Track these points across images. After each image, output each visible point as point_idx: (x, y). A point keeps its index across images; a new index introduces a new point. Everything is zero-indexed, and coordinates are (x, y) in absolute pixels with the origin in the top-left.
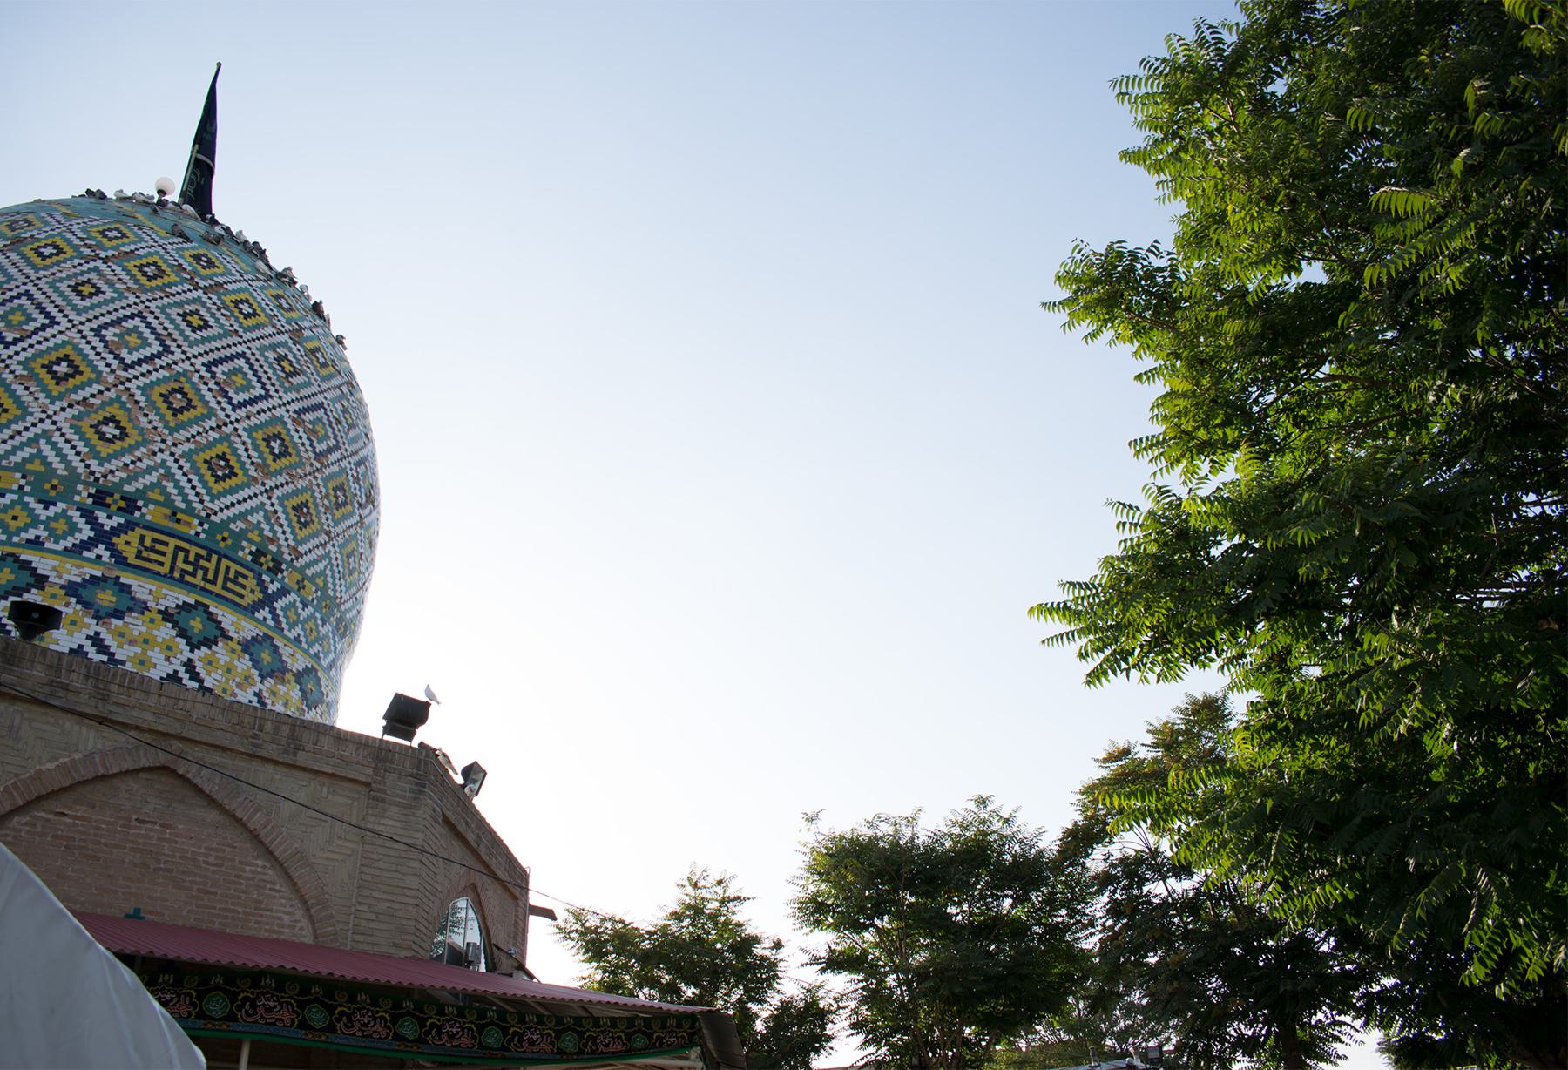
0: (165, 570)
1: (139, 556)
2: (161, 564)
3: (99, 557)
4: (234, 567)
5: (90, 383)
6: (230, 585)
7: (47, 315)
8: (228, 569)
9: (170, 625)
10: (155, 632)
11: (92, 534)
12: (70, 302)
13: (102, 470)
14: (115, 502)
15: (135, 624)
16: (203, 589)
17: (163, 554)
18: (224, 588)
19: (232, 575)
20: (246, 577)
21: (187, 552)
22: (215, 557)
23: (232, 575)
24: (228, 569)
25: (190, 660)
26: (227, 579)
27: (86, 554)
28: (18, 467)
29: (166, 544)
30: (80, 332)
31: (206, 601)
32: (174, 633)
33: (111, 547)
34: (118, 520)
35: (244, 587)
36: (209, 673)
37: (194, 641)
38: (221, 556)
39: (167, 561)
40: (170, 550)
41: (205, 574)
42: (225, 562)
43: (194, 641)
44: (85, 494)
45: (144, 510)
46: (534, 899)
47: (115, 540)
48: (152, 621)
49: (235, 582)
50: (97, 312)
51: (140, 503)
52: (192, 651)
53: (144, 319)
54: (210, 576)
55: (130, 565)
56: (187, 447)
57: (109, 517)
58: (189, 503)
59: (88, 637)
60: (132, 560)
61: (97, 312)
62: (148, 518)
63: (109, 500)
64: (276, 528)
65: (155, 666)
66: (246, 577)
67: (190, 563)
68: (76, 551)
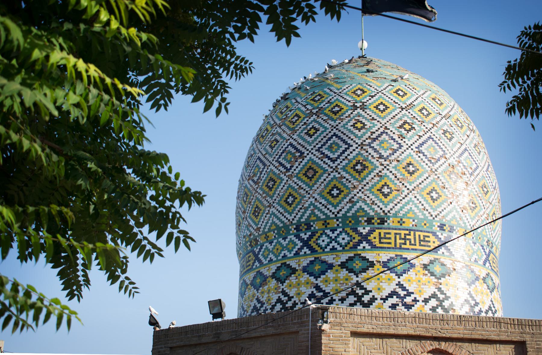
0: (393, 245)
1: (380, 243)
2: (390, 243)
3: (364, 247)
4: (422, 234)
5: (322, 175)
6: (422, 243)
7: (346, 143)
8: (419, 236)
9: (345, 270)
10: (339, 275)
11: (310, 243)
12: (352, 133)
13: (337, 210)
14: (303, 227)
15: (330, 274)
16: (413, 249)
17: (390, 238)
18: (420, 245)
19: (422, 238)
20: (429, 237)
21: (400, 234)
22: (412, 233)
23: (422, 238)
24: (419, 236)
25: (317, 284)
26: (420, 241)
27: (359, 247)
28: (270, 230)
29: (389, 233)
30: (357, 143)
31: (399, 253)
32: (347, 272)
33: (369, 242)
34: (368, 229)
35: (429, 242)
36: (410, 286)
37: (357, 271)
38: (414, 230)
39: (392, 241)
40: (392, 236)
41: (410, 242)
42: (417, 233)
43: (317, 275)
44: (293, 229)
45: (314, 226)
46: (206, 318)
47: (359, 238)
48: (337, 270)
49: (424, 241)
50: (319, 139)
51: (312, 223)
52: (399, 278)
53: (337, 136)
54: (413, 242)
55: (378, 247)
56: (269, 200)
57: (305, 234)
58: (326, 214)
59: (397, 285)
60: (379, 245)
61: (319, 139)
62: (317, 228)
63: (301, 228)
64: (425, 212)
65: (384, 289)
66: (429, 237)
67: (408, 239)
68: (297, 254)
